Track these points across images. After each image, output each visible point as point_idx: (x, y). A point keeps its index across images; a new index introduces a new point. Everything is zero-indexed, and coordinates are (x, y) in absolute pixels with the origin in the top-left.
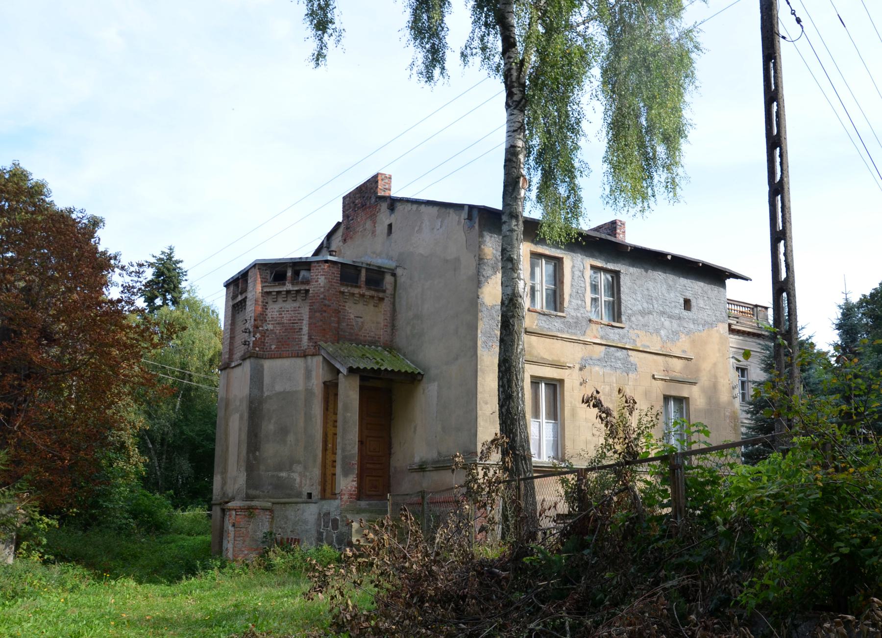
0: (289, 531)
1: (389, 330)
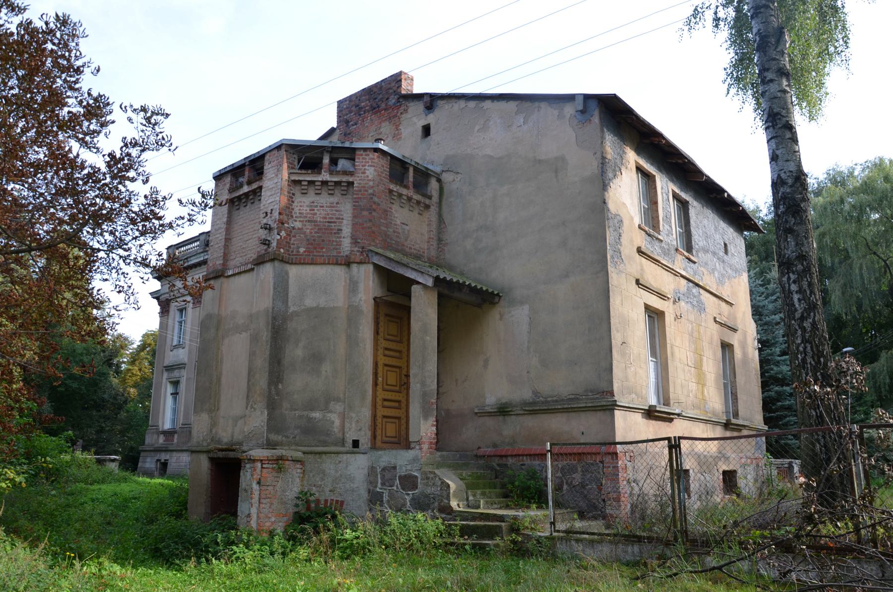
0: (327, 490)
1: (435, 243)
